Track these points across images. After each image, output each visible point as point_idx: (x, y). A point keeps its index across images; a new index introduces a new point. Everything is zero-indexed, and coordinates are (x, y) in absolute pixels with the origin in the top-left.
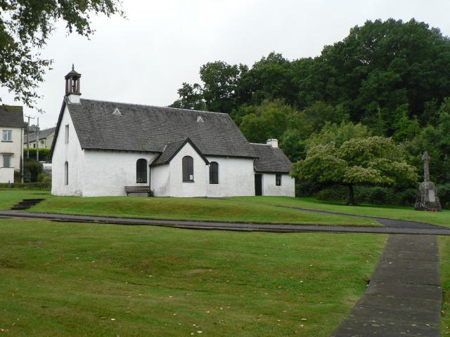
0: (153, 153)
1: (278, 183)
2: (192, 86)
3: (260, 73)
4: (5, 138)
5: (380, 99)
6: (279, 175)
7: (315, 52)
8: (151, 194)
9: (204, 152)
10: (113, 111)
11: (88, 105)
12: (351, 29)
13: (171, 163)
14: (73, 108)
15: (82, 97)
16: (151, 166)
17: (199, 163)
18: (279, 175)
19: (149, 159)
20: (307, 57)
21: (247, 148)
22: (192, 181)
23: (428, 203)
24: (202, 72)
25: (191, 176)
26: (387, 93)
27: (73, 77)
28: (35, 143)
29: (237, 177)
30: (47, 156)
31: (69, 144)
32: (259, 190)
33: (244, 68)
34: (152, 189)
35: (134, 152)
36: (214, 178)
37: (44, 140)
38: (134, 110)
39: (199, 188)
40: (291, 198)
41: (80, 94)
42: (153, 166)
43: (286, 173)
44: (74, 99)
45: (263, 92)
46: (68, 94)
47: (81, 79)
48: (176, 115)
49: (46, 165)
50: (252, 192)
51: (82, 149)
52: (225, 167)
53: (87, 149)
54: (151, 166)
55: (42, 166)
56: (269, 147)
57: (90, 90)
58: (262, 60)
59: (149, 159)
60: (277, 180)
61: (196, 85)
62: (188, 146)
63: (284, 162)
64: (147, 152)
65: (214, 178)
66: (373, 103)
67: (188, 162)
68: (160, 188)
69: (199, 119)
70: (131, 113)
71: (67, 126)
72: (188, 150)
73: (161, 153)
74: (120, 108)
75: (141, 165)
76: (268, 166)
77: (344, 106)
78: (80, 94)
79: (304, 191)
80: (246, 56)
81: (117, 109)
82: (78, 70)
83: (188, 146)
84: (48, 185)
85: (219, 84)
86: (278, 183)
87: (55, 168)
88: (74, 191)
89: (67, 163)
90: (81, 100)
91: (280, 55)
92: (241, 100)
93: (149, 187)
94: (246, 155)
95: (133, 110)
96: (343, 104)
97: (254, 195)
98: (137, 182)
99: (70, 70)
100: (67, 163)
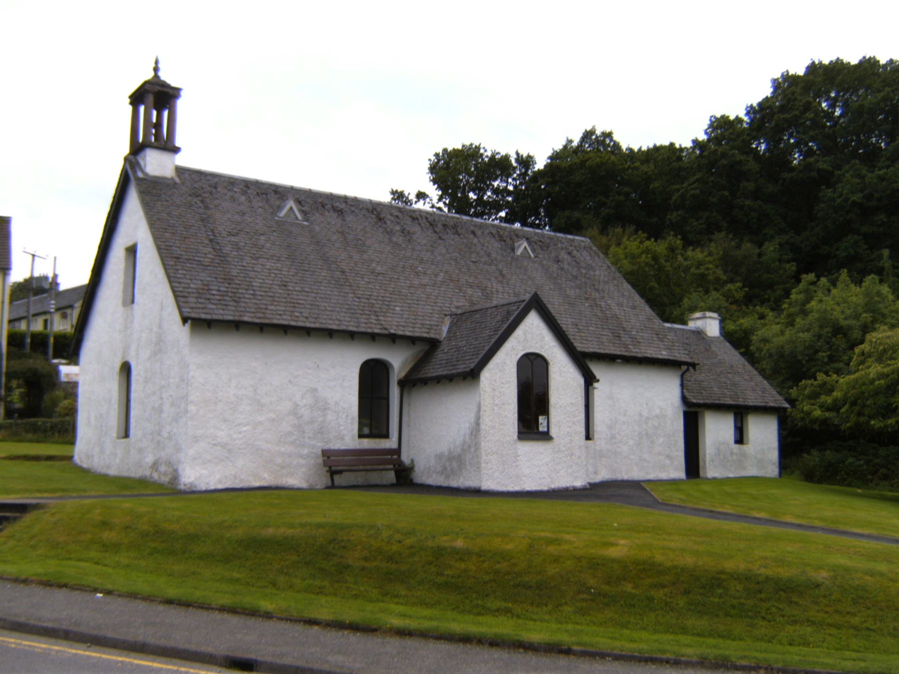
2: (412, 197)
3: (571, 170)
5: (865, 229)
6: (741, 413)
7: (686, 131)
8: (404, 478)
9: (580, 346)
10: (280, 208)
11: (203, 186)
12: (774, 81)
14: (153, 190)
15: (181, 160)
16: (402, 384)
17: (564, 377)
18: (741, 413)
19: (398, 361)
20: (764, 97)
21: (660, 336)
22: (546, 436)
24: (433, 169)
25: (542, 419)
26: (882, 217)
27: (156, 97)
28: (48, 317)
29: (632, 421)
30: (70, 347)
31: (135, 306)
33: (526, 162)
34: (405, 458)
35: (351, 336)
37: (69, 311)
38: (340, 212)
40: (673, 482)
41: (176, 150)
42: (407, 384)
44: (156, 164)
45: (576, 214)
46: (137, 149)
47: (182, 105)
48: (457, 233)
49: (66, 371)
50: (679, 473)
51: (185, 320)
53: (201, 324)
54: (402, 384)
55: (57, 372)
56: (699, 334)
57: (204, 144)
58: (565, 147)
59: (398, 361)
60: (736, 427)
61: (421, 196)
62: (533, 322)
63: (756, 388)
64: (393, 339)
66: (851, 238)
67: (533, 372)
68: (439, 457)
69: (522, 246)
70: (332, 218)
71: (132, 251)
73: (433, 344)
74: (299, 202)
75: (373, 378)
76: (716, 394)
77: (780, 245)
78: (176, 150)
80: (535, 136)
81: (291, 204)
83: (533, 322)
84: (66, 431)
85: (472, 195)
87: (89, 376)
88: (150, 459)
89: (126, 369)
90: (180, 170)
91: (609, 135)
93: (398, 451)
94: (664, 354)
95: (335, 209)
96: (777, 240)
98: (361, 436)
99: (150, 75)
100: (126, 369)
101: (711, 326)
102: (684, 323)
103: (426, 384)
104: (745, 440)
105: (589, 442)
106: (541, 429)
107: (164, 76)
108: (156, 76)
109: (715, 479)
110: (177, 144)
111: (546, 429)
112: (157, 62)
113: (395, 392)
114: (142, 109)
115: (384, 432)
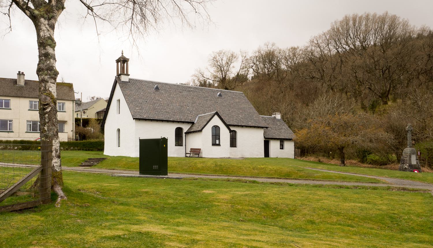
0: (188, 123)
1: (282, 147)
4: (31, 107)
6: (282, 141)
13: (203, 130)
14: (124, 85)
15: (130, 77)
18: (282, 141)
23: (411, 166)
27: (123, 61)
32: (267, 153)
35: (173, 122)
36: (233, 143)
37: (86, 111)
39: (224, 151)
41: (129, 75)
43: (290, 140)
44: (124, 78)
46: (119, 75)
50: (263, 155)
51: (134, 119)
52: (241, 133)
57: (136, 72)
59: (186, 128)
63: (285, 132)
64: (183, 122)
65: (233, 143)
67: (216, 128)
71: (119, 101)
72: (216, 121)
78: (129, 75)
79: (303, 151)
82: (126, 56)
86: (282, 147)
89: (119, 130)
90: (130, 79)
92: (278, 87)
97: (264, 157)
99: (120, 55)
101: (278, 116)
102: (271, 116)
103: (191, 133)
104: (284, 148)
105: (233, 149)
106: (217, 143)
107: (125, 55)
108: (122, 55)
109: (272, 158)
110: (129, 74)
111: (218, 143)
112: (122, 51)
113: (184, 135)
114: (119, 63)
115: (182, 145)
